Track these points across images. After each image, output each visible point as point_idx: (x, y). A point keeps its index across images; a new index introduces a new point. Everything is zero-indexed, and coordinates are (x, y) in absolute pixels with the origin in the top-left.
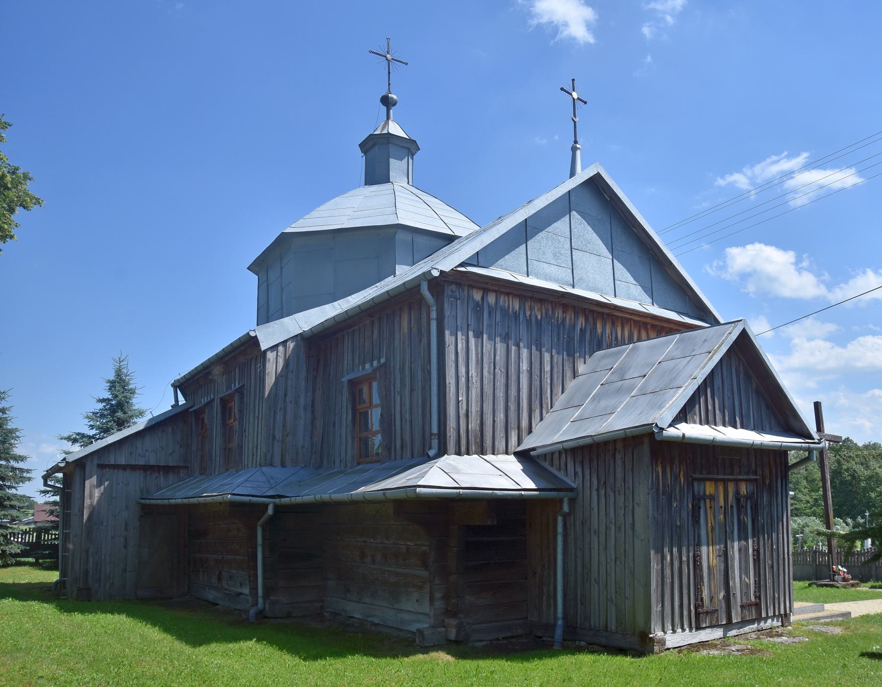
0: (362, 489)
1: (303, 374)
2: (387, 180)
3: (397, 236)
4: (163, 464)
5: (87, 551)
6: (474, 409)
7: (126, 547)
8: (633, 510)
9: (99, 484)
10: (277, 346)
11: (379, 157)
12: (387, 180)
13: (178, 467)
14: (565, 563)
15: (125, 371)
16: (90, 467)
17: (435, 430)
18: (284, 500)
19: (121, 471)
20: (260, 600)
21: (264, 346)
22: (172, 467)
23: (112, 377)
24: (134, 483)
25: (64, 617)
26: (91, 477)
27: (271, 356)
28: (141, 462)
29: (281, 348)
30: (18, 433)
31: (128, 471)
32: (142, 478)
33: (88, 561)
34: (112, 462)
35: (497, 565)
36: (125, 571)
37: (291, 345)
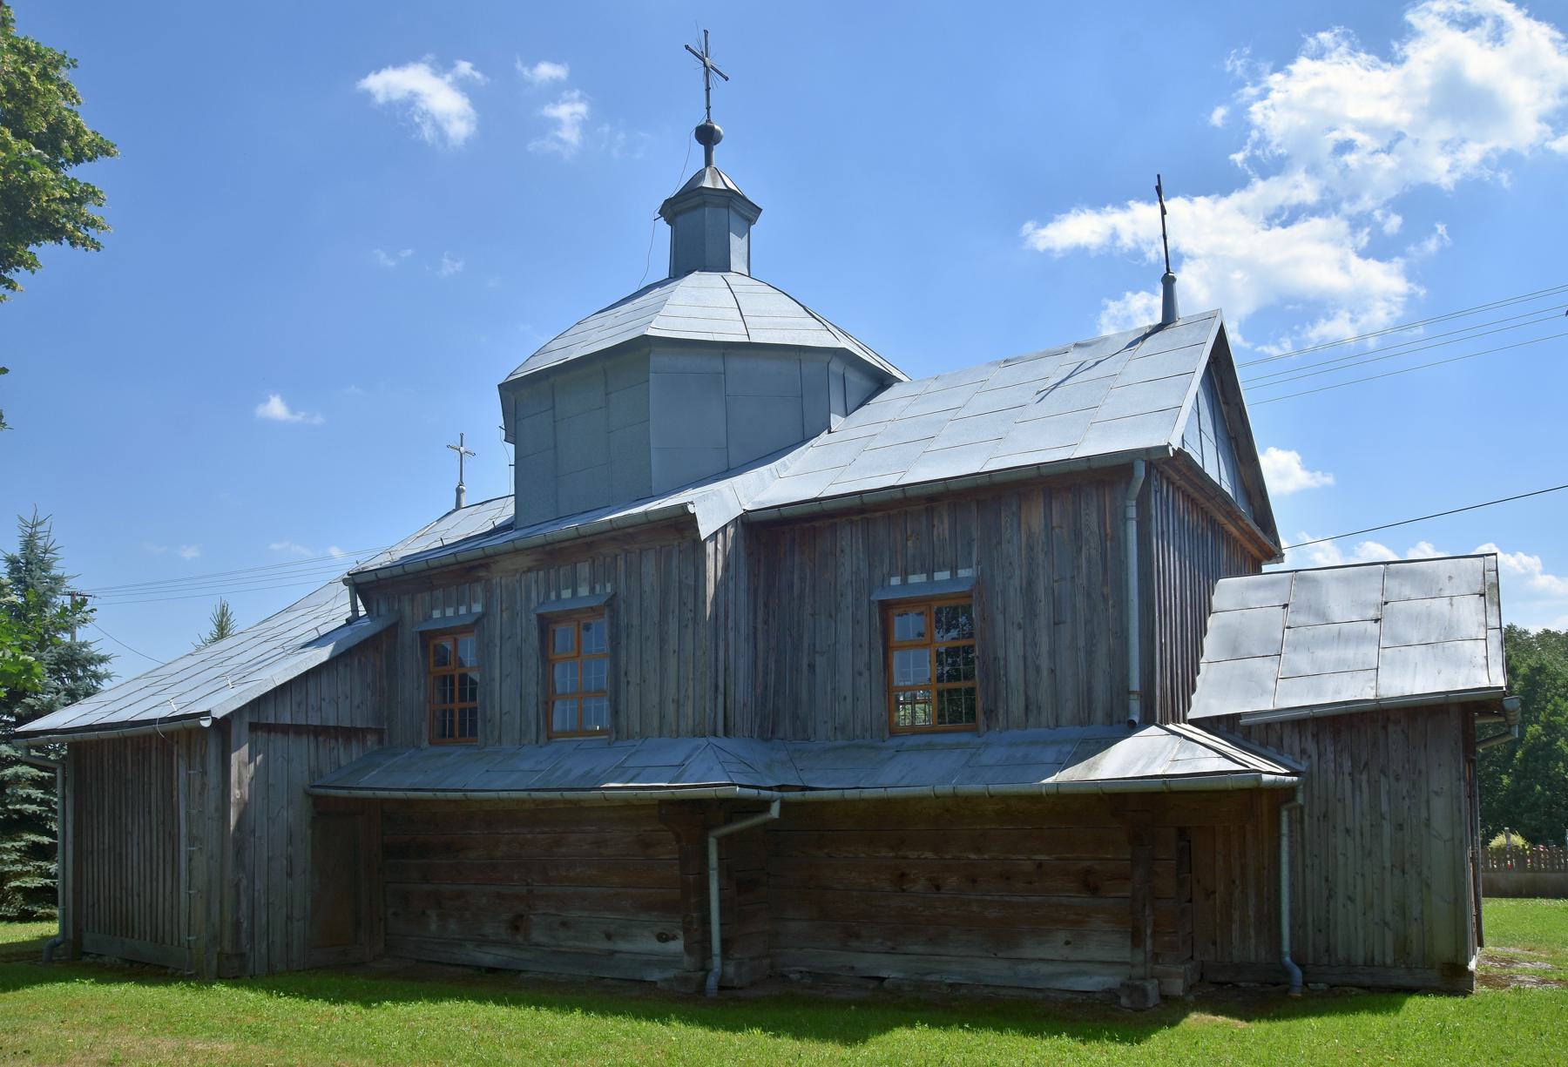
0: (1050, 780)
1: (743, 585)
2: (725, 267)
3: (652, 358)
4: (347, 724)
5: (237, 886)
6: (673, 626)
7: (290, 875)
8: (1428, 801)
9: (251, 758)
10: (716, 533)
11: (702, 227)
12: (725, 267)
13: (365, 731)
14: (1292, 885)
15: (41, 543)
16: (239, 730)
17: (1135, 685)
18: (809, 795)
19: (280, 735)
20: (716, 962)
21: (704, 532)
22: (362, 730)
23: (16, 550)
24: (300, 757)
25: (1138, 1049)
26: (239, 748)
27: (710, 547)
28: (314, 720)
29: (720, 536)
30: (101, 669)
31: (291, 736)
32: (312, 746)
33: (238, 902)
34: (272, 720)
35: (1219, 890)
36: (289, 918)
37: (731, 531)
